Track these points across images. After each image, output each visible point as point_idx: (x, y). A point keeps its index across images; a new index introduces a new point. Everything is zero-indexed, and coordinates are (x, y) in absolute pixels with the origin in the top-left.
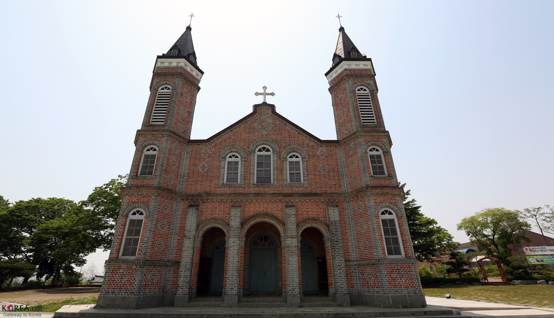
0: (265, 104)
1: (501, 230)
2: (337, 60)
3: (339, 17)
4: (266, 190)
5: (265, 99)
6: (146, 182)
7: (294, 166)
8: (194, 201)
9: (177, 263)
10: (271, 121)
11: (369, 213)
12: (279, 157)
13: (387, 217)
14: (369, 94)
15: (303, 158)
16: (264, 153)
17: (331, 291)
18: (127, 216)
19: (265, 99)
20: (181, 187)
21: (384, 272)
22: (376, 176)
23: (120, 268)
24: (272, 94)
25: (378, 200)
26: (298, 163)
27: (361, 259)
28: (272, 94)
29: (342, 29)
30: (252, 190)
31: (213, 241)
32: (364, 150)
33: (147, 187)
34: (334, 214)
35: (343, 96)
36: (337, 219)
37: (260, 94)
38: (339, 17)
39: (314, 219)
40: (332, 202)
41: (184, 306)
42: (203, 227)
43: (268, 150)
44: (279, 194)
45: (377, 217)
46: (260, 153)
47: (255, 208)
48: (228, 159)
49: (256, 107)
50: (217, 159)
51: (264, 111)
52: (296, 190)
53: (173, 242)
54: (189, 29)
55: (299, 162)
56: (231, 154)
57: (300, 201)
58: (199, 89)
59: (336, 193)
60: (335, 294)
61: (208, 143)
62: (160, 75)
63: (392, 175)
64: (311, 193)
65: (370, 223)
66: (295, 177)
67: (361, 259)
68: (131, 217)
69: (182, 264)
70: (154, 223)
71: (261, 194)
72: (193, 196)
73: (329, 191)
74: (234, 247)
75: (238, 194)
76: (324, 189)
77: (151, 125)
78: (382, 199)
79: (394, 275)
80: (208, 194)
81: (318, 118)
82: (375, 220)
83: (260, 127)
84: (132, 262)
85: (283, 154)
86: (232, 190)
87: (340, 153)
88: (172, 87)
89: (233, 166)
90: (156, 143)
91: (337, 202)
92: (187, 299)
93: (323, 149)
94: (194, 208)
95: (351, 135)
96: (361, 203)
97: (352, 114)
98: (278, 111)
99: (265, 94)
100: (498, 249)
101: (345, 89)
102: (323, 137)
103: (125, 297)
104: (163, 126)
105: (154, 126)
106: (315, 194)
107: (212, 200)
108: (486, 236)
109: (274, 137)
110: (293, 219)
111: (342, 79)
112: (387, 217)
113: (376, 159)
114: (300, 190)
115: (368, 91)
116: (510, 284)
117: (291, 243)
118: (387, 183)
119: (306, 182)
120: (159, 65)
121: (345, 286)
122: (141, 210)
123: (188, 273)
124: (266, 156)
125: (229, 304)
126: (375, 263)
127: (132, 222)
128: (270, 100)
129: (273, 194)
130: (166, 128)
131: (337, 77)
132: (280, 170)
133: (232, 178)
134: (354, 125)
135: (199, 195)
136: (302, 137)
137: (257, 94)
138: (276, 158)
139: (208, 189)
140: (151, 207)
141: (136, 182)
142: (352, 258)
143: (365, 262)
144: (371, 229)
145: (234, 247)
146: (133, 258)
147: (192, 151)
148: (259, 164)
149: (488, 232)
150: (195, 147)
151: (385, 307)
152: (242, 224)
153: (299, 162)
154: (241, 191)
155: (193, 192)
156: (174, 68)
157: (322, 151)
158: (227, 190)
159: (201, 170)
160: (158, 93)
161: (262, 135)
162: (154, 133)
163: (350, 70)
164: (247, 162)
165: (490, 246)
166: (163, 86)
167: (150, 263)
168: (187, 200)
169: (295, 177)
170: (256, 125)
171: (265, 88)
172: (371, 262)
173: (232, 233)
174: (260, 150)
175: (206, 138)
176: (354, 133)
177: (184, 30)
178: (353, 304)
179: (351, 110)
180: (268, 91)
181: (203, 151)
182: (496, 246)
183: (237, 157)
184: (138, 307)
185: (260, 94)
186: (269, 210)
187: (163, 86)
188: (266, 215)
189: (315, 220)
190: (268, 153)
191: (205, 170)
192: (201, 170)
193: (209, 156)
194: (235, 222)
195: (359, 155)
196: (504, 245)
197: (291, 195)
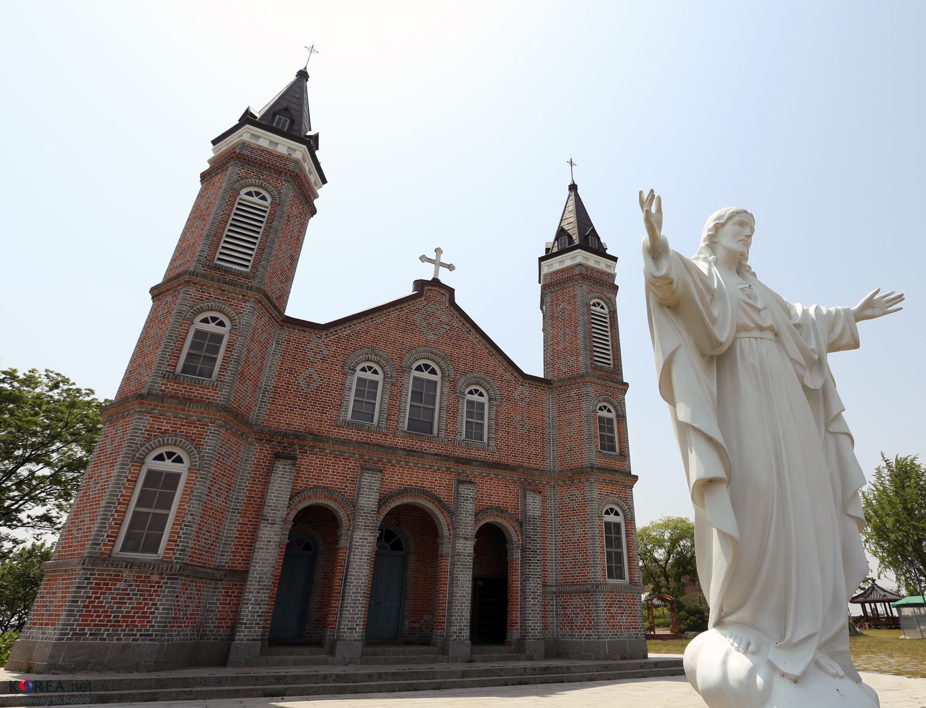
0: (436, 282)
1: (678, 553)
2: (564, 242)
3: (571, 163)
4: (425, 445)
5: (437, 272)
6: (196, 392)
7: (475, 410)
8: (286, 447)
9: (238, 576)
10: (444, 318)
11: (589, 509)
12: (453, 389)
13: (611, 518)
14: (608, 316)
15: (490, 400)
16: (425, 375)
17: (514, 634)
18: (142, 462)
19: (437, 272)
20: (258, 413)
21: (602, 604)
22: (604, 452)
23: (117, 578)
24: (451, 267)
25: (604, 491)
26: (482, 405)
27: (566, 584)
28: (451, 267)
29: (573, 187)
30: (400, 442)
31: (315, 531)
32: (591, 403)
33: (199, 402)
34: (534, 504)
35: (569, 308)
36: (538, 513)
37: (430, 260)
38: (571, 163)
39: (501, 511)
40: (529, 484)
41: (249, 664)
42: (300, 502)
43: (433, 372)
44: (448, 458)
45: (600, 517)
46: (419, 374)
47: (402, 476)
48: (359, 374)
49: (420, 285)
50: (339, 368)
51: (432, 293)
52: (474, 454)
53: (231, 527)
54: (303, 75)
55: (376, 383)
56: (366, 364)
57: (480, 474)
58: (313, 212)
59: (537, 470)
60: (523, 638)
61: (324, 333)
62: (553, 288)
63: (624, 455)
64: (498, 464)
65: (588, 525)
66: (474, 430)
67: (566, 584)
68: (151, 464)
69: (253, 577)
70: (208, 483)
71: (415, 451)
72: (285, 435)
73: (526, 464)
74: (360, 548)
75: (373, 445)
76: (519, 460)
77: (218, 268)
78: (608, 489)
79: (613, 610)
80: (317, 437)
81: (521, 337)
82: (597, 522)
83: (424, 324)
84: (154, 566)
85: (460, 384)
86: (362, 436)
87: (549, 401)
88: (273, 197)
89: (366, 389)
90: (228, 309)
91: (537, 485)
92: (258, 650)
93: (522, 391)
94: (289, 462)
95: (575, 378)
96: (577, 492)
97: (580, 342)
98: (458, 301)
99: (438, 264)
100: (668, 582)
101: (574, 297)
102: (527, 371)
103: (126, 647)
104: (246, 276)
105: (227, 271)
106: (506, 467)
107: (322, 450)
108: (656, 561)
109: (448, 350)
110: (469, 507)
111: (571, 279)
112: (611, 518)
113: (605, 424)
114: (481, 455)
115: (606, 311)
116: (681, 638)
117: (460, 549)
118: (617, 465)
119: (492, 443)
120: (545, 270)
121: (539, 626)
122: (179, 452)
123: (264, 596)
124: (428, 381)
125: (345, 658)
126: (589, 591)
127: (153, 476)
128: (445, 277)
129: (435, 455)
130: (254, 283)
131: (562, 271)
132: (453, 413)
133: (364, 412)
134: (582, 362)
135: (298, 436)
136: (493, 362)
137: (423, 259)
138: (446, 390)
139: (315, 426)
140: (207, 449)
141: (172, 387)
142: (549, 582)
143: (572, 589)
144: (589, 536)
145: (360, 548)
146: (149, 557)
147: (288, 341)
148: (416, 395)
149: (660, 554)
150: (297, 334)
151: (597, 659)
152: (382, 501)
153: (376, 383)
154: (380, 440)
155: (283, 427)
156: (280, 157)
157: (522, 393)
158: (353, 435)
159: (303, 384)
160: (238, 200)
161: (427, 342)
162: (227, 287)
163: (587, 267)
164: (394, 384)
165: (659, 577)
166: (252, 189)
167: (191, 571)
168: (269, 441)
169: (474, 430)
170: (418, 318)
171: (438, 251)
172: (583, 588)
173: (361, 521)
174: (419, 369)
175: (322, 320)
176: (582, 376)
177: (292, 77)
178: (547, 657)
179: (580, 335)
180: (443, 259)
181: (311, 345)
182: (667, 578)
183: (375, 372)
184: (158, 666)
185: (430, 260)
186: (427, 485)
187: (252, 189)
188: (423, 492)
189: (502, 511)
190: (432, 377)
191: (313, 386)
192: (303, 384)
193: (324, 359)
194: (368, 500)
195: (584, 413)
196: (678, 578)
197: (467, 462)
